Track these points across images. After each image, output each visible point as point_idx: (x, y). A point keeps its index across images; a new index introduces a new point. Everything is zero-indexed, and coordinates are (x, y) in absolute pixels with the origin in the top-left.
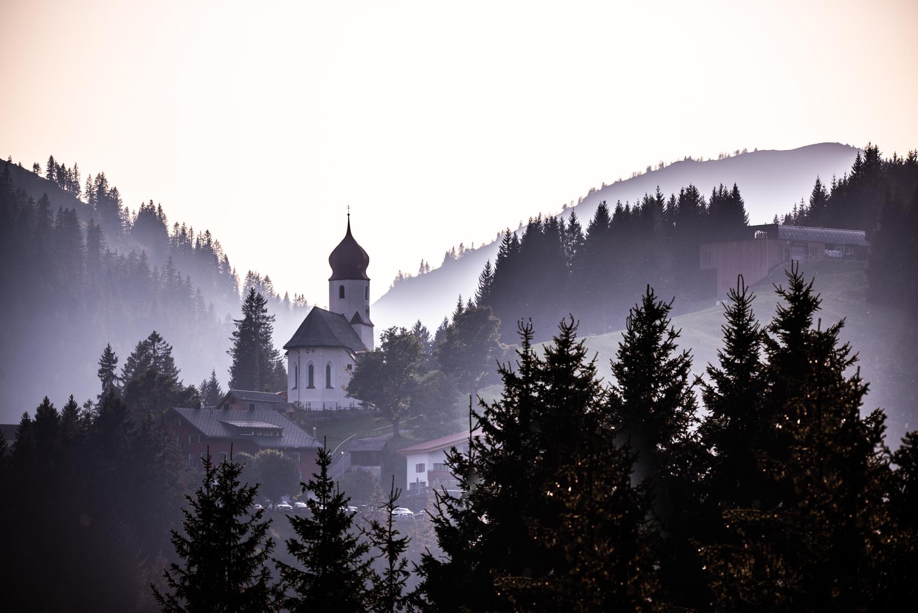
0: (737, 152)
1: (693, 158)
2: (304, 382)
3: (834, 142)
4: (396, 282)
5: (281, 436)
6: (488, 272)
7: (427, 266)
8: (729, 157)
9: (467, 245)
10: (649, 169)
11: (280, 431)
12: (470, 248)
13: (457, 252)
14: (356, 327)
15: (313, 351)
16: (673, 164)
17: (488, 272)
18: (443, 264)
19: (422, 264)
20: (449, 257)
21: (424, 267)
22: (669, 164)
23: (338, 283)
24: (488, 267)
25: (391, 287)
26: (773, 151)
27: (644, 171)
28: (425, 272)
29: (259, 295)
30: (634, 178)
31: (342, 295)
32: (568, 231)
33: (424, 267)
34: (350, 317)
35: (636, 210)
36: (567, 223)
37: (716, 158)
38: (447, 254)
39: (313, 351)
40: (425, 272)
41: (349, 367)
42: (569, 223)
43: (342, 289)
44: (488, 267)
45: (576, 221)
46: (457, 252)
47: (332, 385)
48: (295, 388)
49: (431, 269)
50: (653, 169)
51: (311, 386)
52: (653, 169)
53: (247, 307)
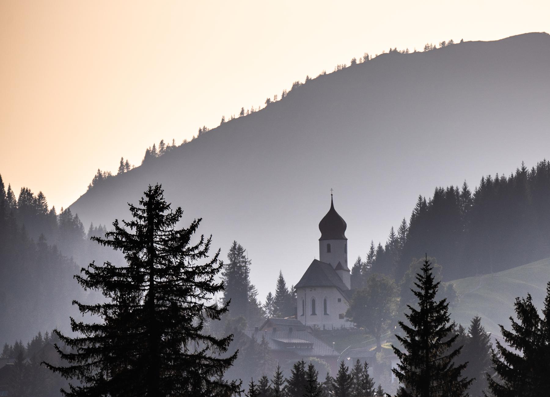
0: (443, 43)
1: (398, 50)
2: (309, 311)
3: (541, 31)
4: (95, 181)
5: (312, 348)
6: (404, 226)
7: (127, 164)
8: (435, 48)
9: (168, 143)
10: (354, 62)
11: (311, 345)
12: (171, 145)
13: (158, 150)
14: (338, 272)
15: (315, 289)
16: (377, 57)
17: (404, 226)
18: (144, 162)
19: (122, 163)
20: (150, 154)
21: (124, 165)
22: (374, 57)
23: (326, 242)
24: (404, 223)
25: (90, 187)
26: (479, 41)
27: (349, 64)
28: (125, 171)
29: (239, 246)
30: (339, 71)
31: (329, 250)
32: (462, 196)
33: (124, 165)
34: (335, 265)
35: (511, 180)
36: (461, 191)
37: (422, 50)
38: (148, 152)
39: (315, 289)
40: (125, 171)
41: (339, 300)
42: (462, 190)
43: (329, 246)
44: (404, 223)
45: (468, 189)
46: (158, 150)
47: (328, 313)
48: (303, 315)
49: (131, 168)
50: (358, 62)
51: (314, 313)
52: (358, 62)
53: (231, 255)
